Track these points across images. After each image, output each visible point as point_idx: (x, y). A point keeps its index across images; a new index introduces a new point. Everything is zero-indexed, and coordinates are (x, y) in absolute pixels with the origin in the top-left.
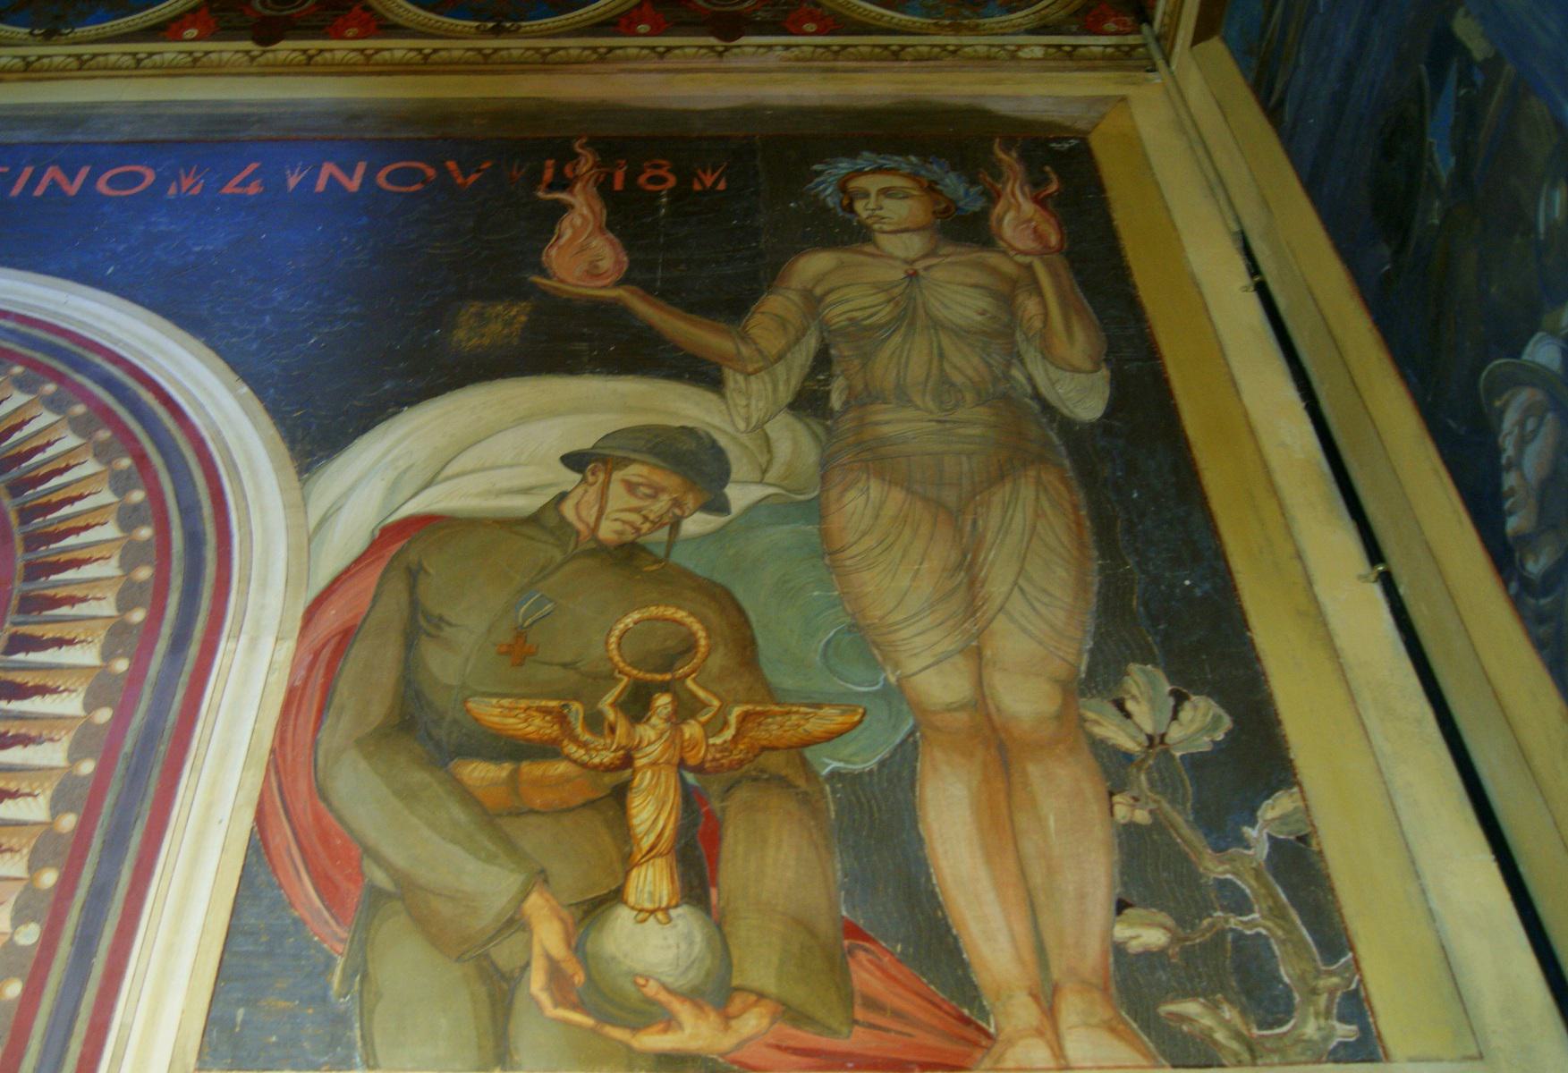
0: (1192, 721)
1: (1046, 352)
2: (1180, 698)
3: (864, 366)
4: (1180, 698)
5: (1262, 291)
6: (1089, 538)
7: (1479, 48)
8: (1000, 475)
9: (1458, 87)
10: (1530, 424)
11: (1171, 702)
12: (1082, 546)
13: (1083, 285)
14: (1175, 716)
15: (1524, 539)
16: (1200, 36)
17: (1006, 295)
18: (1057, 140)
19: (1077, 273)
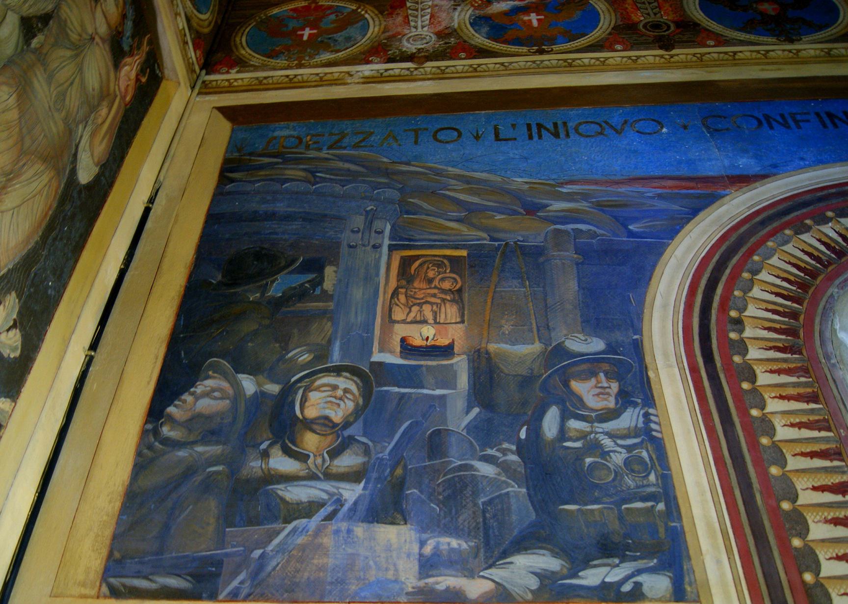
0: (10, 339)
1: (93, 135)
2: (14, 326)
3: (53, 46)
4: (14, 326)
5: (147, 211)
6: (43, 226)
7: (328, 284)
8: (45, 160)
9: (308, 282)
10: (216, 394)
11: (11, 323)
12: (40, 224)
13: (120, 128)
14: (8, 330)
15: (171, 419)
16: (228, 112)
17: (105, 95)
18: (159, 67)
19: (122, 122)
